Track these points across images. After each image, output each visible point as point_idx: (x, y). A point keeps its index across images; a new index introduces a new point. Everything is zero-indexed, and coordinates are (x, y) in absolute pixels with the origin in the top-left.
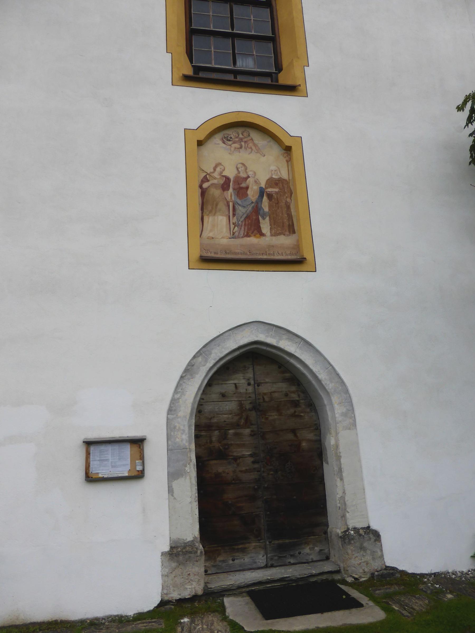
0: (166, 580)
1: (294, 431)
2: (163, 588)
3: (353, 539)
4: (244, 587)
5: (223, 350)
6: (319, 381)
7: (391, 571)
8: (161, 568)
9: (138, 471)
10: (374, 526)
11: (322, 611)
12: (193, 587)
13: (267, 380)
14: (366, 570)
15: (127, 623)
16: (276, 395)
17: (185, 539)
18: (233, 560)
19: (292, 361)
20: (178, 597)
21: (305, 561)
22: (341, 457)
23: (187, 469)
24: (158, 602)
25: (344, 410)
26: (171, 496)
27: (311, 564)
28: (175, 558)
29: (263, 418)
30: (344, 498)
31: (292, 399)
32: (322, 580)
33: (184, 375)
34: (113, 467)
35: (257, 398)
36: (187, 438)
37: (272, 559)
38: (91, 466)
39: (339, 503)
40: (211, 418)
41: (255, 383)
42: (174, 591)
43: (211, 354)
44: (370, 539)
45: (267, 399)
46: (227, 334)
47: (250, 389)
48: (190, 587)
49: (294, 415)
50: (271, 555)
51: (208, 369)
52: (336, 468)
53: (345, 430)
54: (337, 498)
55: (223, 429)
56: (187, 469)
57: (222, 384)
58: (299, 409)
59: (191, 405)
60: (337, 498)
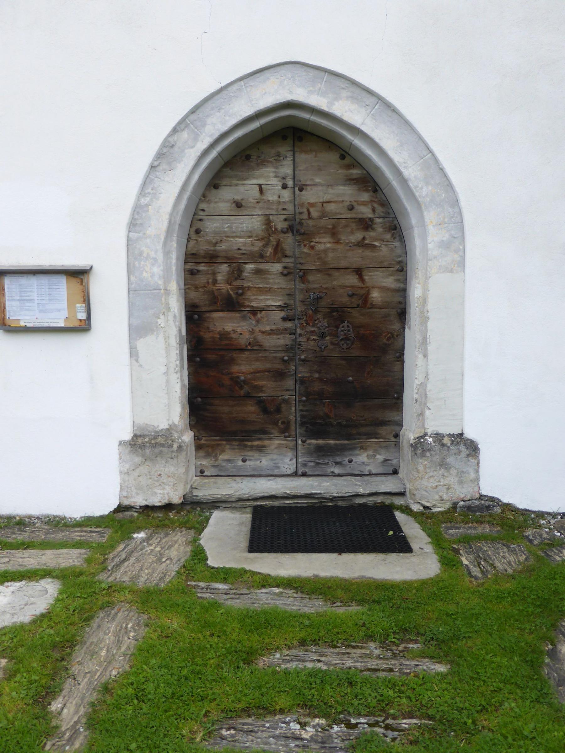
0: (127, 479)
1: (359, 272)
2: (121, 488)
3: (429, 450)
4: (248, 500)
5: (227, 118)
6: (404, 181)
7: (488, 503)
8: (118, 463)
9: (80, 320)
10: (469, 434)
11: (340, 550)
12: (166, 492)
13: (318, 180)
14: (445, 497)
15: (64, 528)
16: (331, 207)
17: (156, 425)
18: (244, 461)
19: (358, 142)
20: (144, 503)
21: (357, 473)
22: (428, 318)
23: (161, 321)
24: (116, 506)
25: (446, 237)
26: (134, 362)
27: (366, 478)
28: (140, 450)
29: (305, 246)
30: (426, 385)
31: (360, 216)
32: (375, 503)
33: (156, 163)
34: (41, 311)
35: (297, 211)
36: (161, 273)
37: (304, 465)
38: (7, 309)
39: (417, 393)
40: (217, 243)
41: (295, 185)
42: (137, 494)
43: (204, 125)
44: (460, 452)
45: (315, 213)
46: (235, 87)
47: (286, 195)
48: (161, 492)
49: (361, 244)
50: (304, 459)
51: (199, 154)
52: (418, 337)
53: (444, 272)
54: (415, 386)
55: (235, 261)
56: (161, 321)
57: (237, 185)
58: (372, 234)
59: (168, 216)
60: (415, 386)
